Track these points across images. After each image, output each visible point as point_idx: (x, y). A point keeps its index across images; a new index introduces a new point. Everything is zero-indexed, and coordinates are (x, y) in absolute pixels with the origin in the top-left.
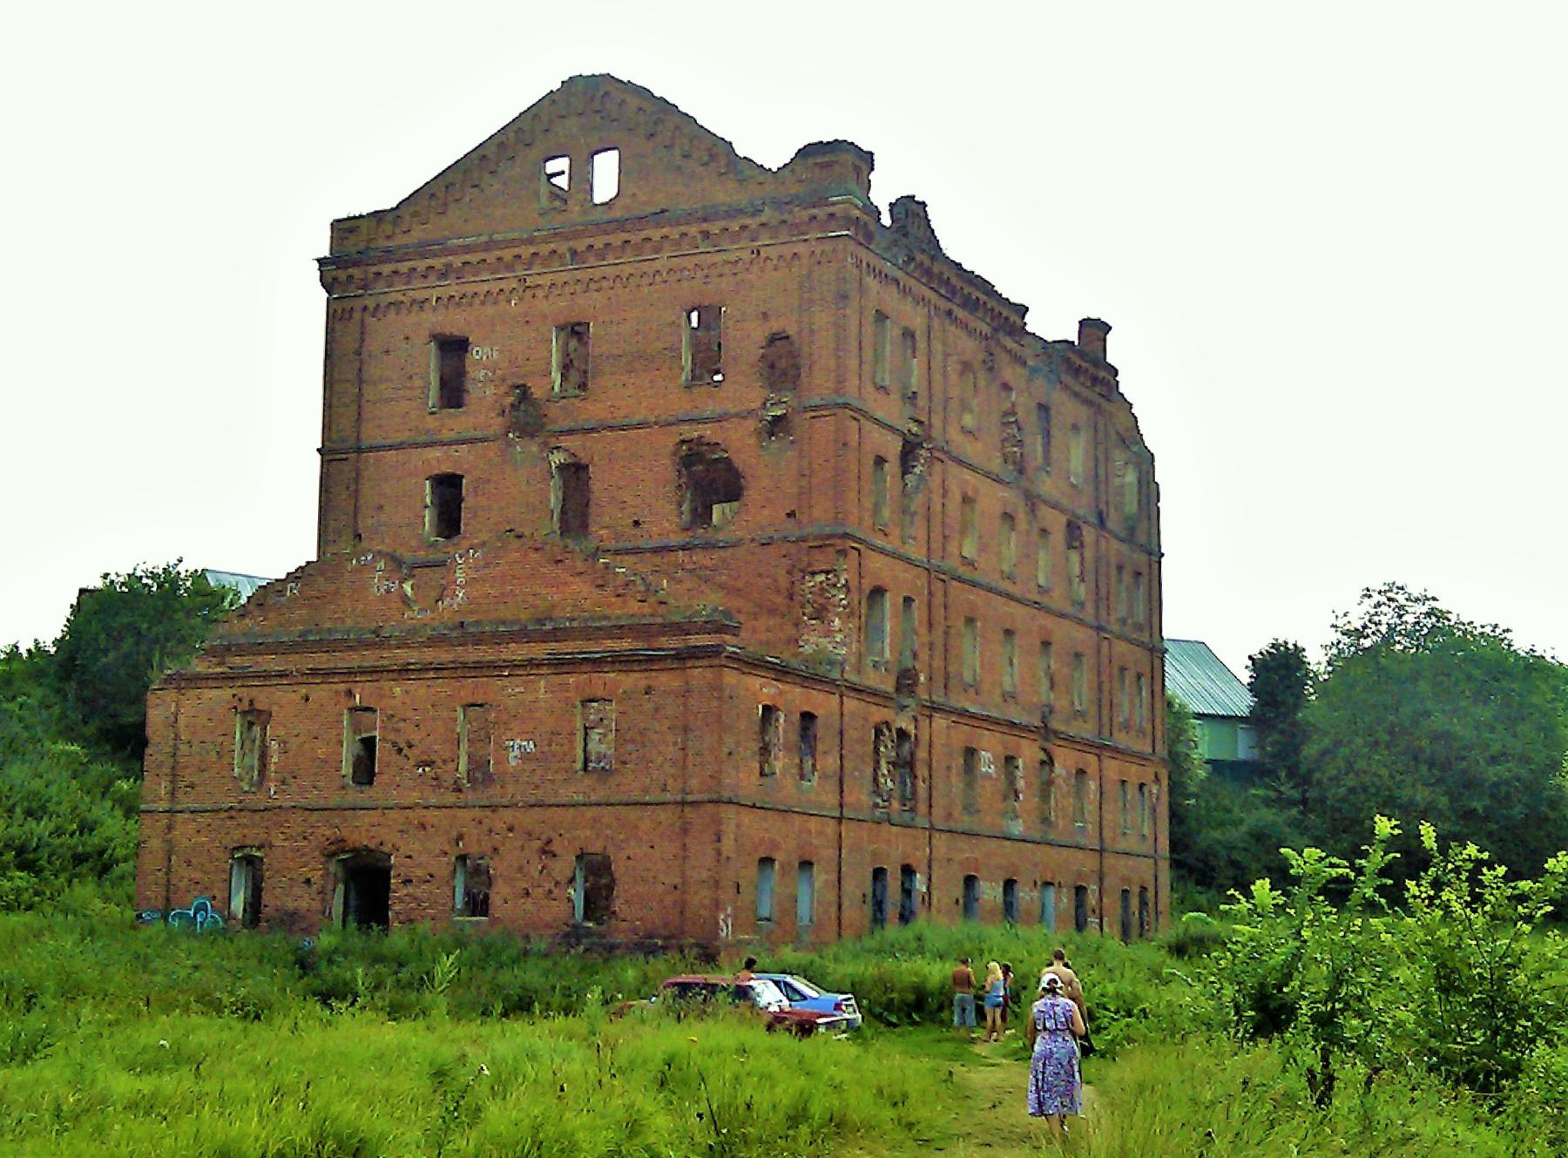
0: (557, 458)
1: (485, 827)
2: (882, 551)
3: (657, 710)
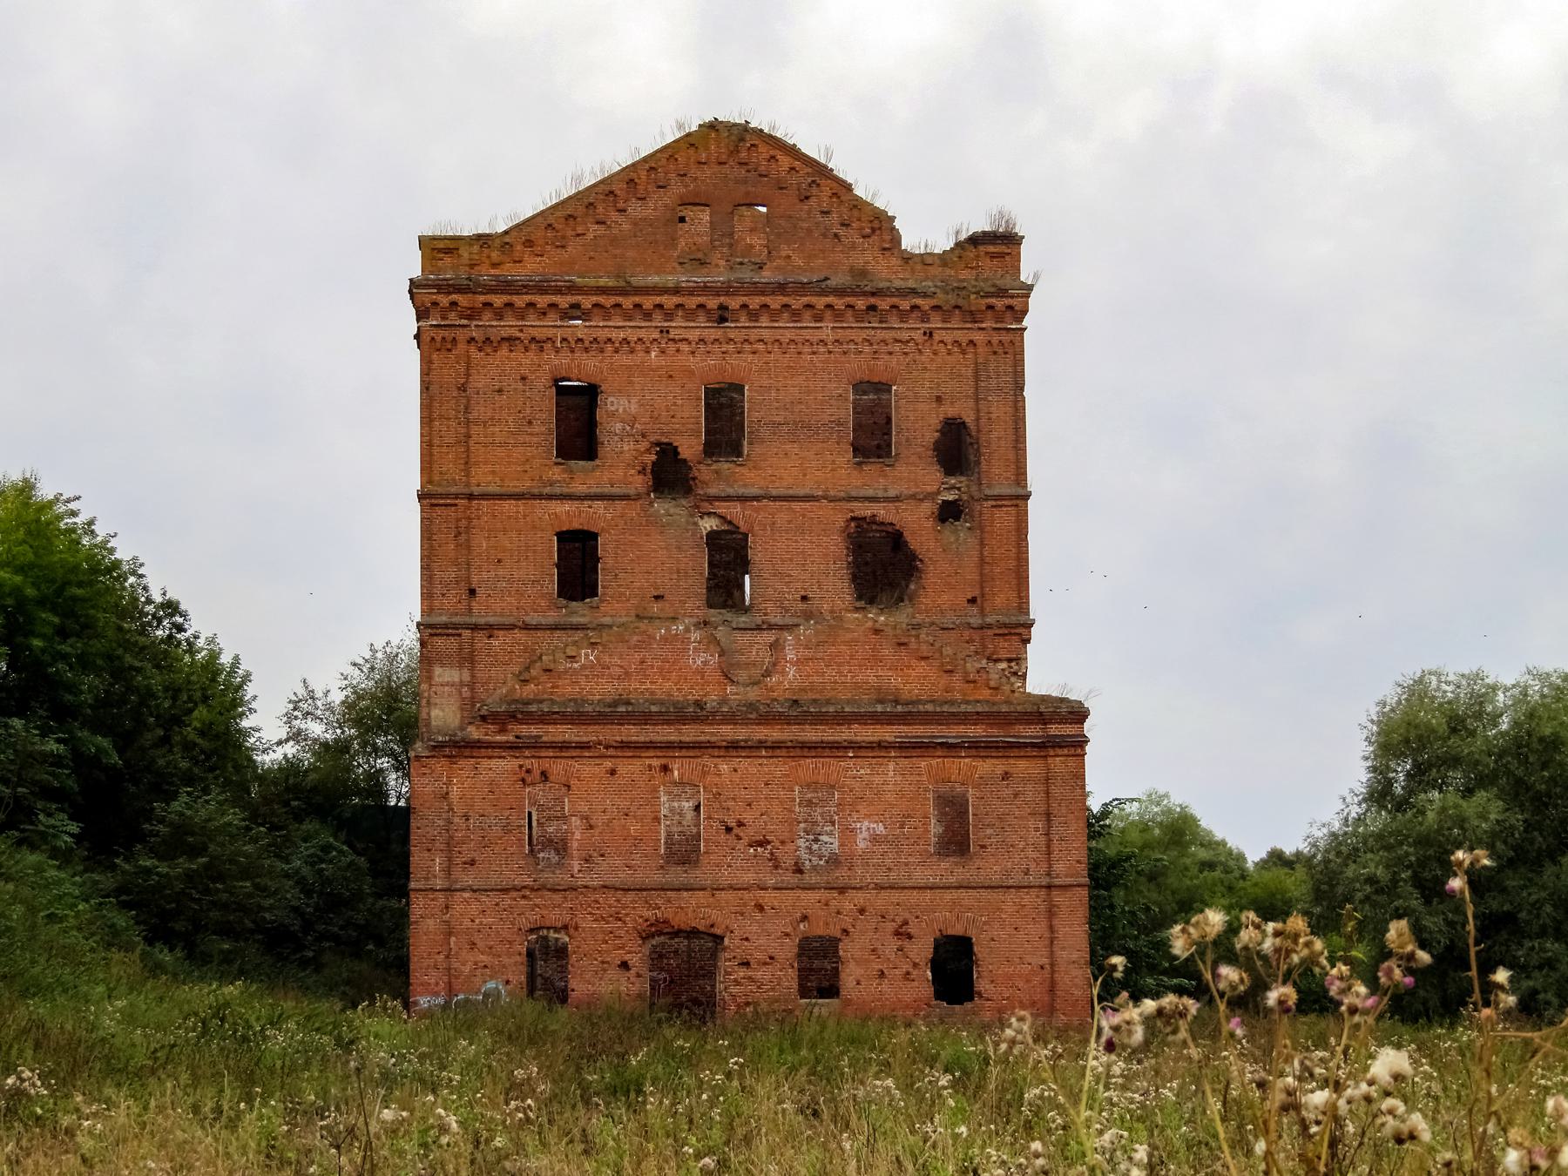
0: (709, 524)
1: (833, 909)
3: (1016, 795)
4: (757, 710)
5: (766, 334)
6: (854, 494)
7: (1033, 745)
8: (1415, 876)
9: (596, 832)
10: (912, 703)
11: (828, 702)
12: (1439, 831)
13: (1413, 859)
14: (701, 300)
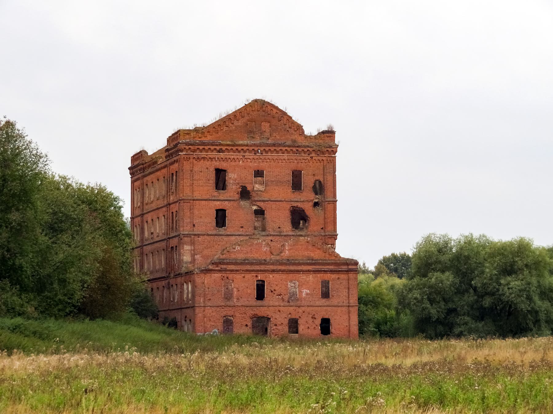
0: (255, 208)
1: (297, 312)
4: (279, 262)
5: (270, 157)
6: (292, 200)
8: (428, 297)
9: (240, 292)
10: (316, 260)
11: (296, 260)
12: (435, 284)
13: (428, 292)
14: (253, 148)
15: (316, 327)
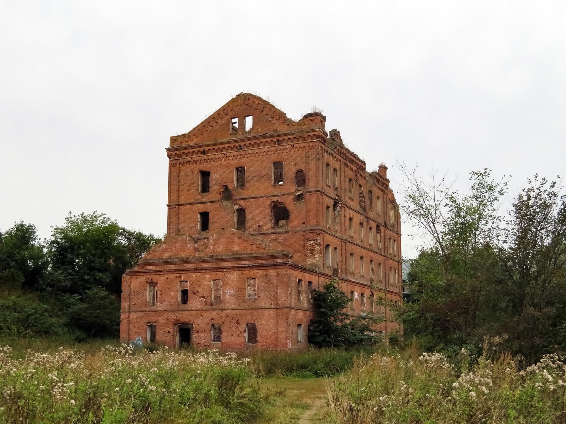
0: (236, 207)
1: (220, 316)
2: (329, 234)
3: (269, 281)
7: (273, 265)
11: (220, 256)
14: (234, 144)
15: (241, 334)
